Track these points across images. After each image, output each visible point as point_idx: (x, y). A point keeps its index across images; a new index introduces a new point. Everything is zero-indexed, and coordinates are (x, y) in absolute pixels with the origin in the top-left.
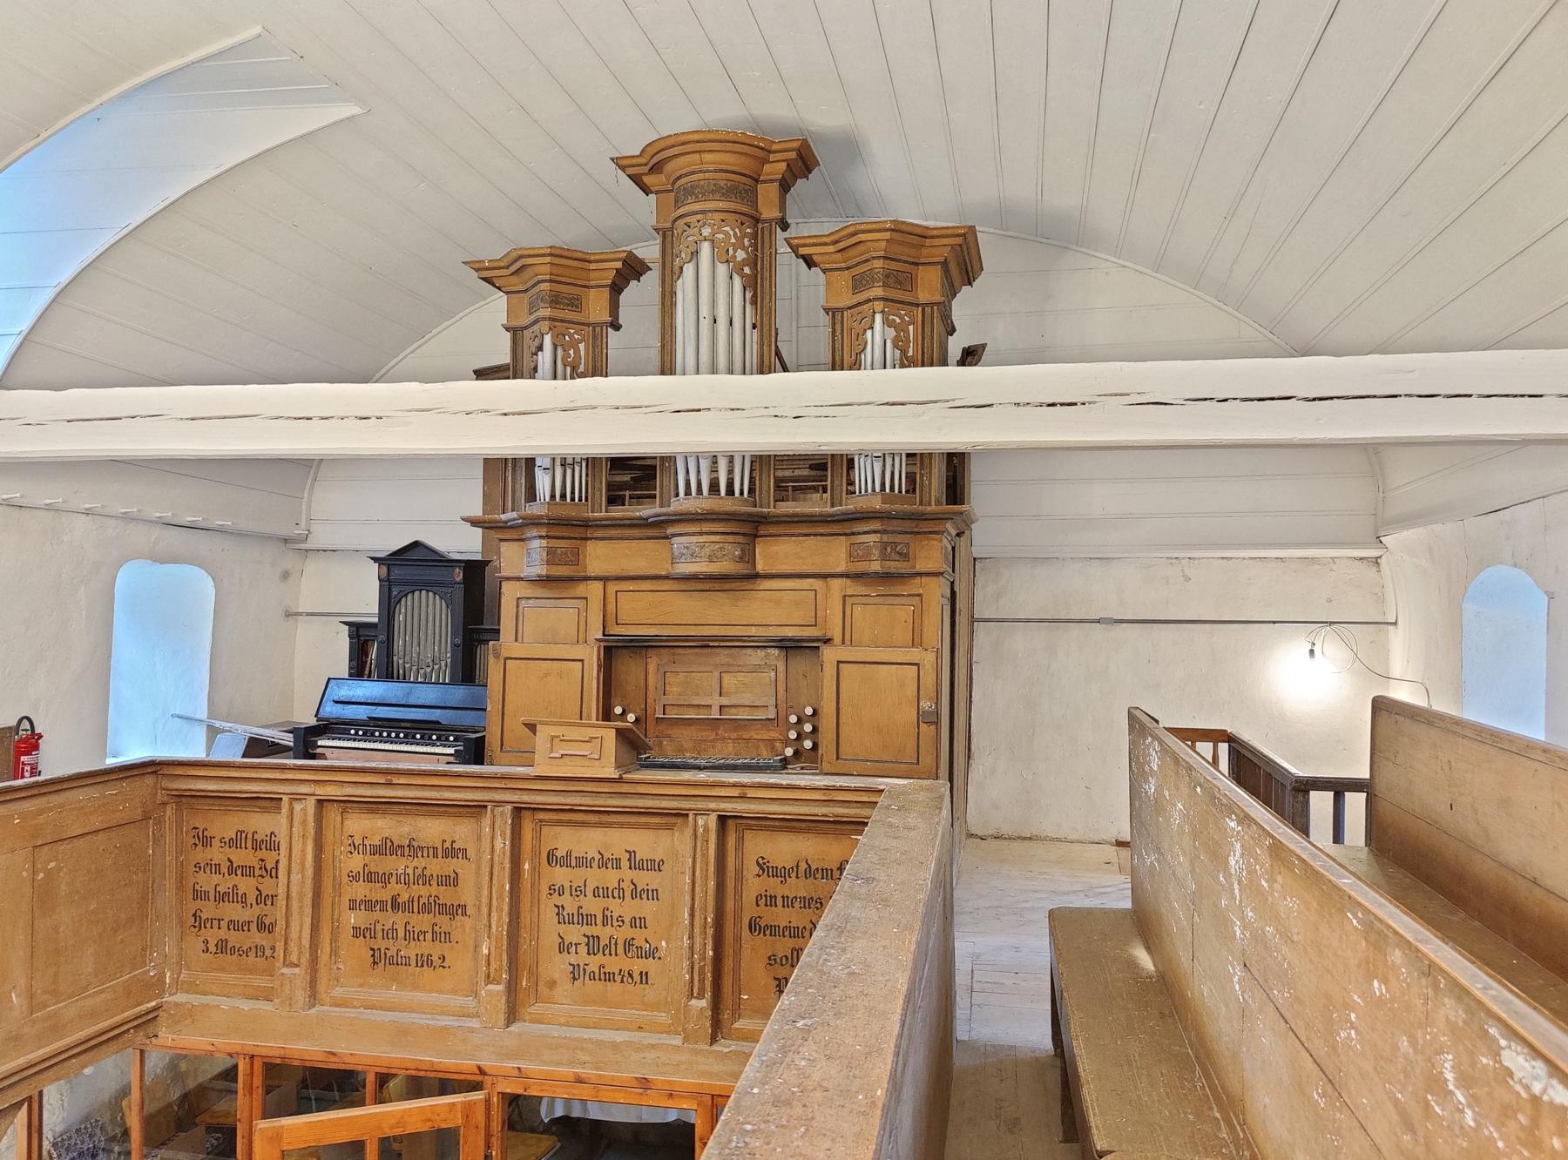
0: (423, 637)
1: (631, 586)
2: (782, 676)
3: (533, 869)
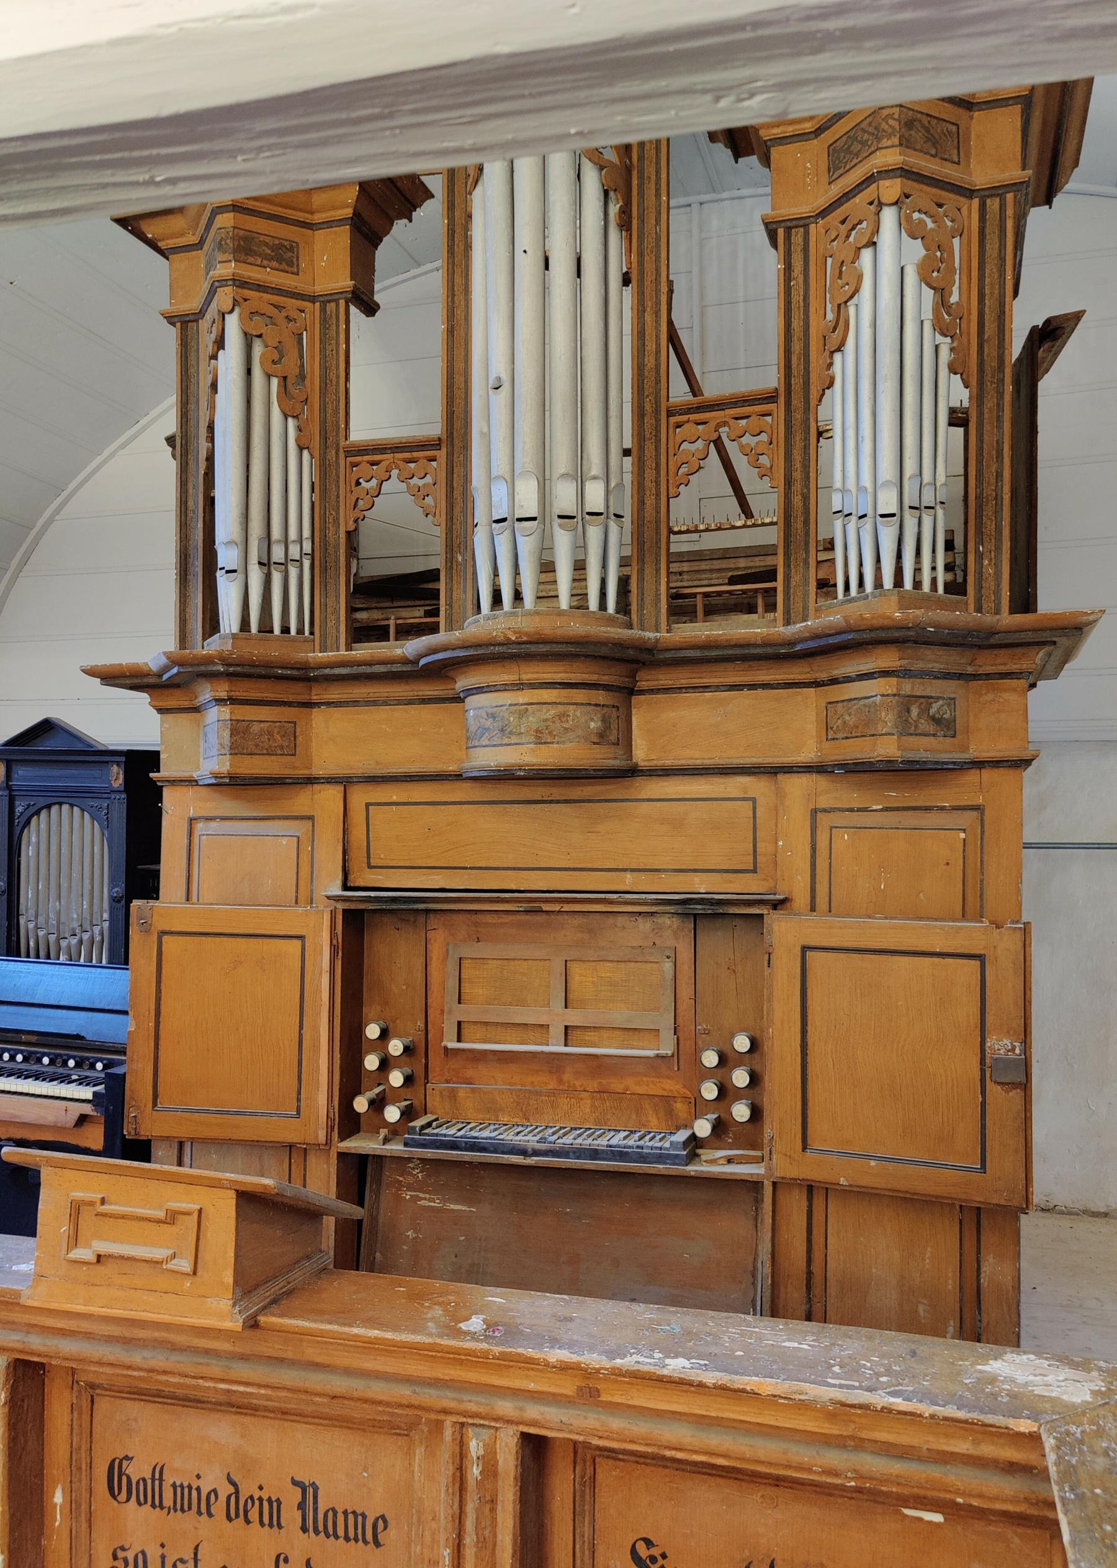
0: (64, 884)
1: (394, 793)
2: (686, 969)
3: (73, 1505)
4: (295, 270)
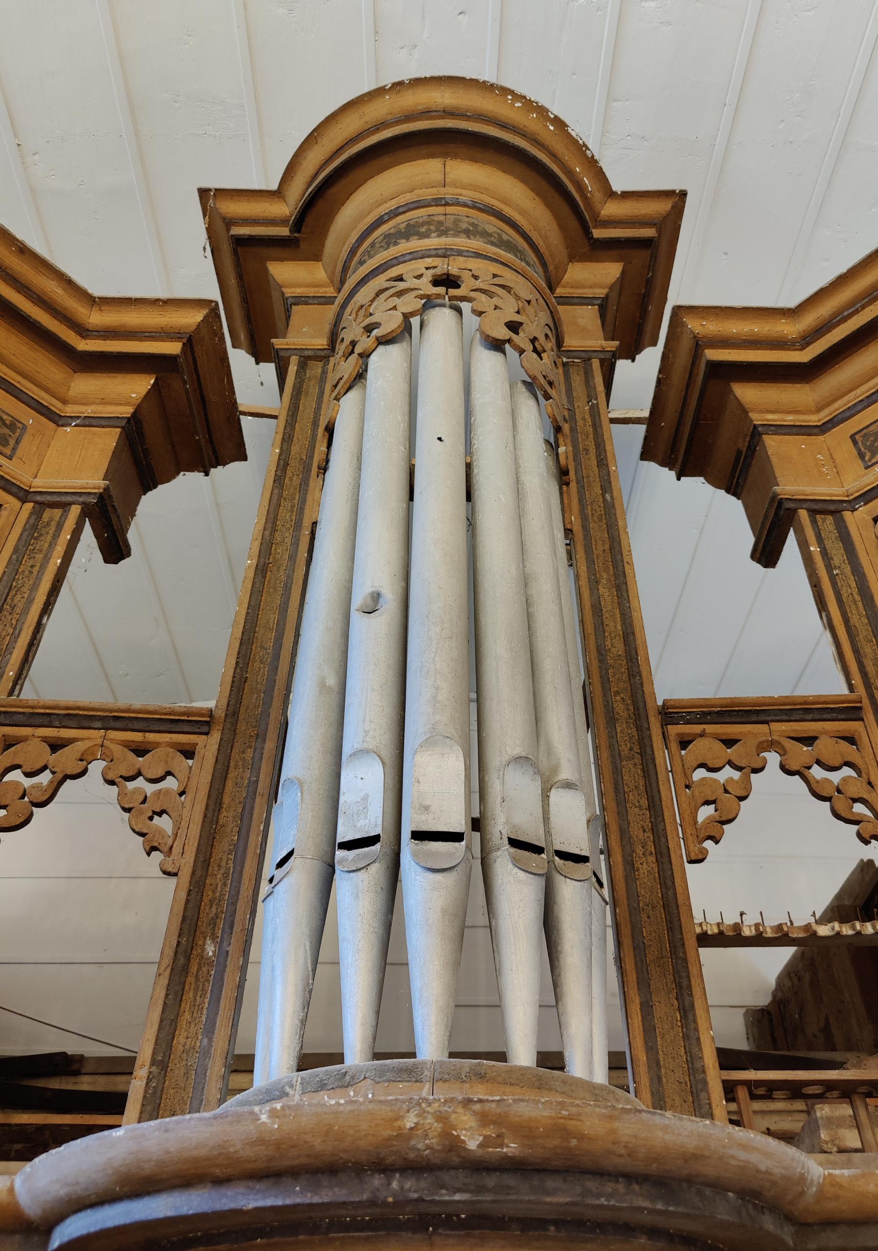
4: (8, 451)
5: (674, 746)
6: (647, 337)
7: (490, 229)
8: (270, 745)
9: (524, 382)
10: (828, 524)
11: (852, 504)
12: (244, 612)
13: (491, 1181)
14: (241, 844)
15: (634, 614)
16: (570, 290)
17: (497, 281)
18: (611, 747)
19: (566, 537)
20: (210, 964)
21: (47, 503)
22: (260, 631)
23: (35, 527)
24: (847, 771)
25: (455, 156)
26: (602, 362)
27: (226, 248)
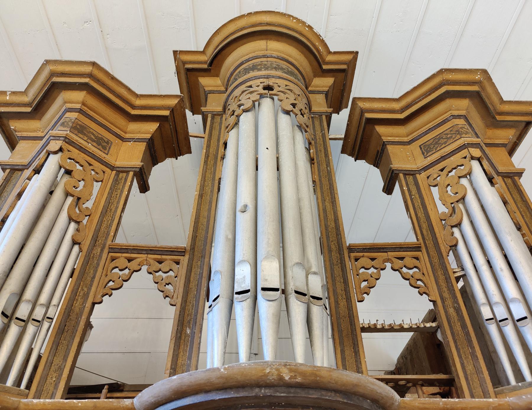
5: (353, 260)
6: (343, 105)
7: (284, 67)
8: (206, 260)
9: (297, 126)
10: (410, 179)
11: (419, 172)
12: (195, 211)
13: (292, 390)
14: (198, 294)
15: (338, 213)
16: (314, 88)
17: (287, 87)
18: (330, 261)
19: (313, 184)
20: (189, 336)
21: (125, 171)
22: (201, 219)
23: (117, 180)
24: (415, 270)
25: (271, 39)
26: (326, 116)
27: (183, 72)
